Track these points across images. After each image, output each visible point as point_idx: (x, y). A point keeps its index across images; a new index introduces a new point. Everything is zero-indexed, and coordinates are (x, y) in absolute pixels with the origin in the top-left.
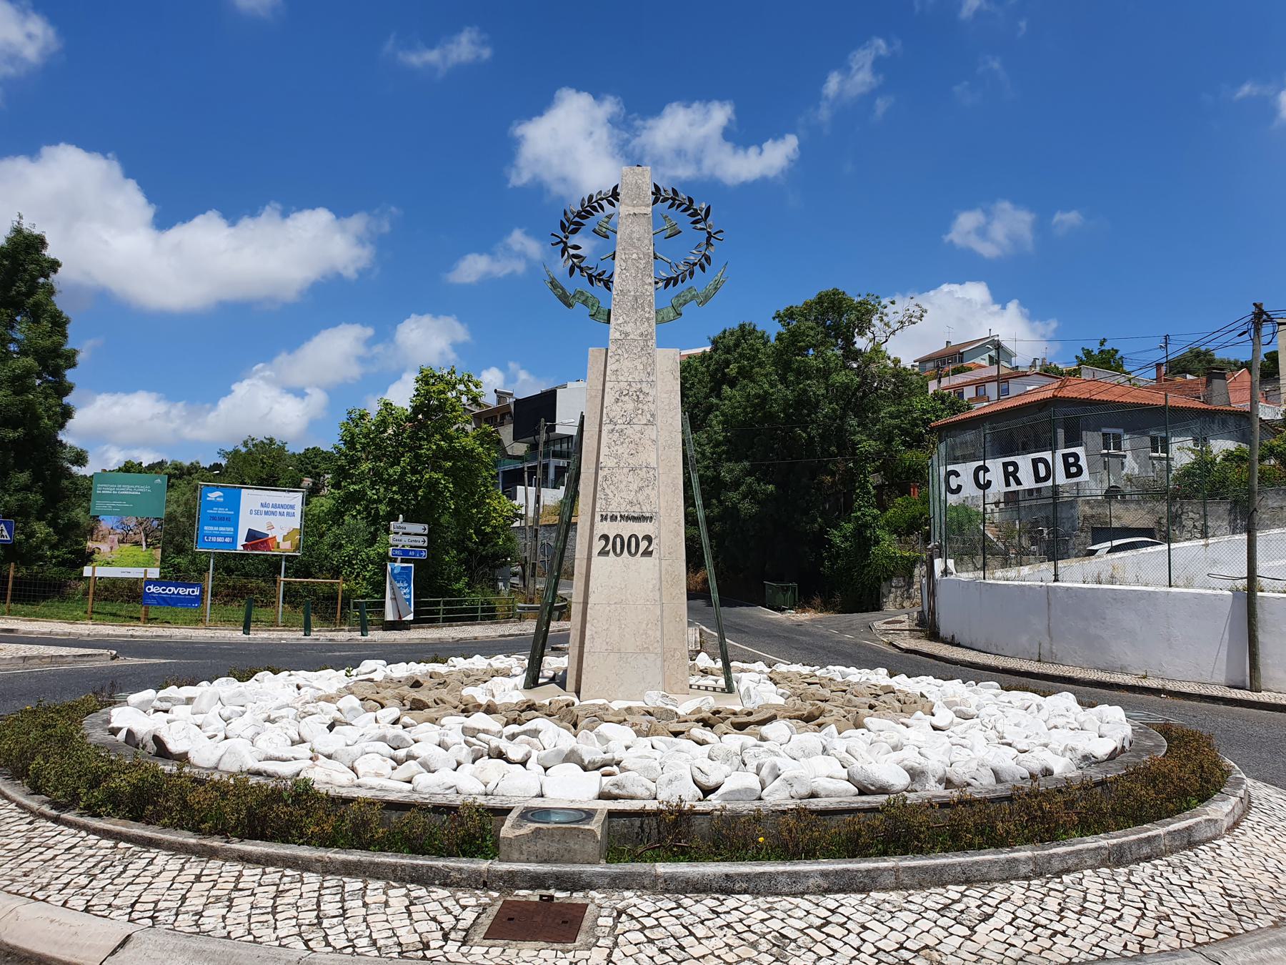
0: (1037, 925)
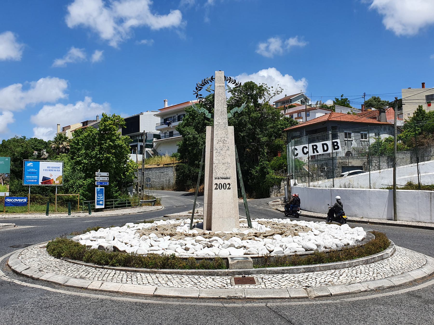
0: (352, 276)
